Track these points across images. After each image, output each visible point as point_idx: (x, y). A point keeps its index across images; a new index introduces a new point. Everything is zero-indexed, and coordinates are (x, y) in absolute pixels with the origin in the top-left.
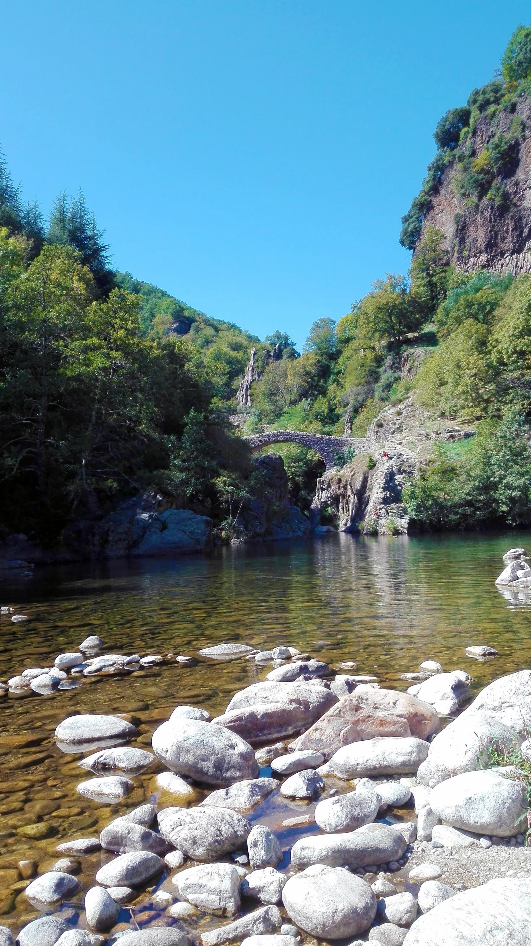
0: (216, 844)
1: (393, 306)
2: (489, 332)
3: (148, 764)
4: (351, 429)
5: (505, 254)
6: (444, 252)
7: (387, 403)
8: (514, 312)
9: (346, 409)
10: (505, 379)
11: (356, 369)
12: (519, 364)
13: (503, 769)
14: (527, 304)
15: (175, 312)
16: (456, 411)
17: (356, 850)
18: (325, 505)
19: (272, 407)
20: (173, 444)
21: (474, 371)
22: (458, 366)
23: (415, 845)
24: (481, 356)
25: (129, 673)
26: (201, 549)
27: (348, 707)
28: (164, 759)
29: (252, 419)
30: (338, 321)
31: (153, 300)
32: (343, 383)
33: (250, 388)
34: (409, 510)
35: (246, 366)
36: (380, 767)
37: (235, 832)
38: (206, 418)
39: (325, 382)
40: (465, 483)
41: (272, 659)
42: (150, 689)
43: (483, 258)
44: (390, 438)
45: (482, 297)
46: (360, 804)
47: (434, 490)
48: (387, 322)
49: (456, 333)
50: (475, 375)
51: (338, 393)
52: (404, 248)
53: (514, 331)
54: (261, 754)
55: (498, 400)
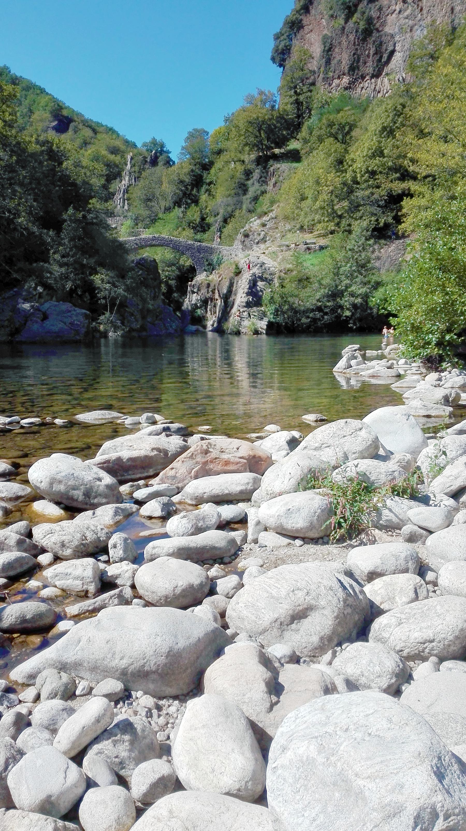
0: (82, 546)
1: (263, 122)
2: (346, 151)
3: (25, 495)
4: (220, 237)
5: (365, 77)
6: (311, 71)
7: (253, 215)
8: (369, 134)
9: (216, 218)
10: (357, 196)
11: (227, 180)
12: (370, 183)
13: (317, 491)
14: (381, 126)
15: (54, 111)
16: (313, 225)
17: (197, 548)
18: (195, 307)
19: (148, 212)
20: (52, 239)
21: (331, 188)
22: (318, 183)
23: (245, 546)
24: (338, 174)
25: (10, 431)
26: (80, 340)
27: (199, 451)
28: (39, 488)
29: (129, 222)
30: (211, 132)
31: (31, 96)
32: (214, 193)
33: (127, 193)
34: (268, 313)
35: (123, 170)
36: (222, 495)
37: (99, 538)
38: (84, 217)
39: (198, 191)
40: (317, 291)
41: (140, 423)
42: (29, 443)
43: (346, 80)
44: (255, 247)
45: (342, 117)
46: (204, 519)
47: (290, 296)
48: (257, 137)
49: (317, 151)
50: (332, 192)
51: (210, 203)
52: (275, 66)
53: (368, 152)
54: (125, 489)
55: (350, 216)
